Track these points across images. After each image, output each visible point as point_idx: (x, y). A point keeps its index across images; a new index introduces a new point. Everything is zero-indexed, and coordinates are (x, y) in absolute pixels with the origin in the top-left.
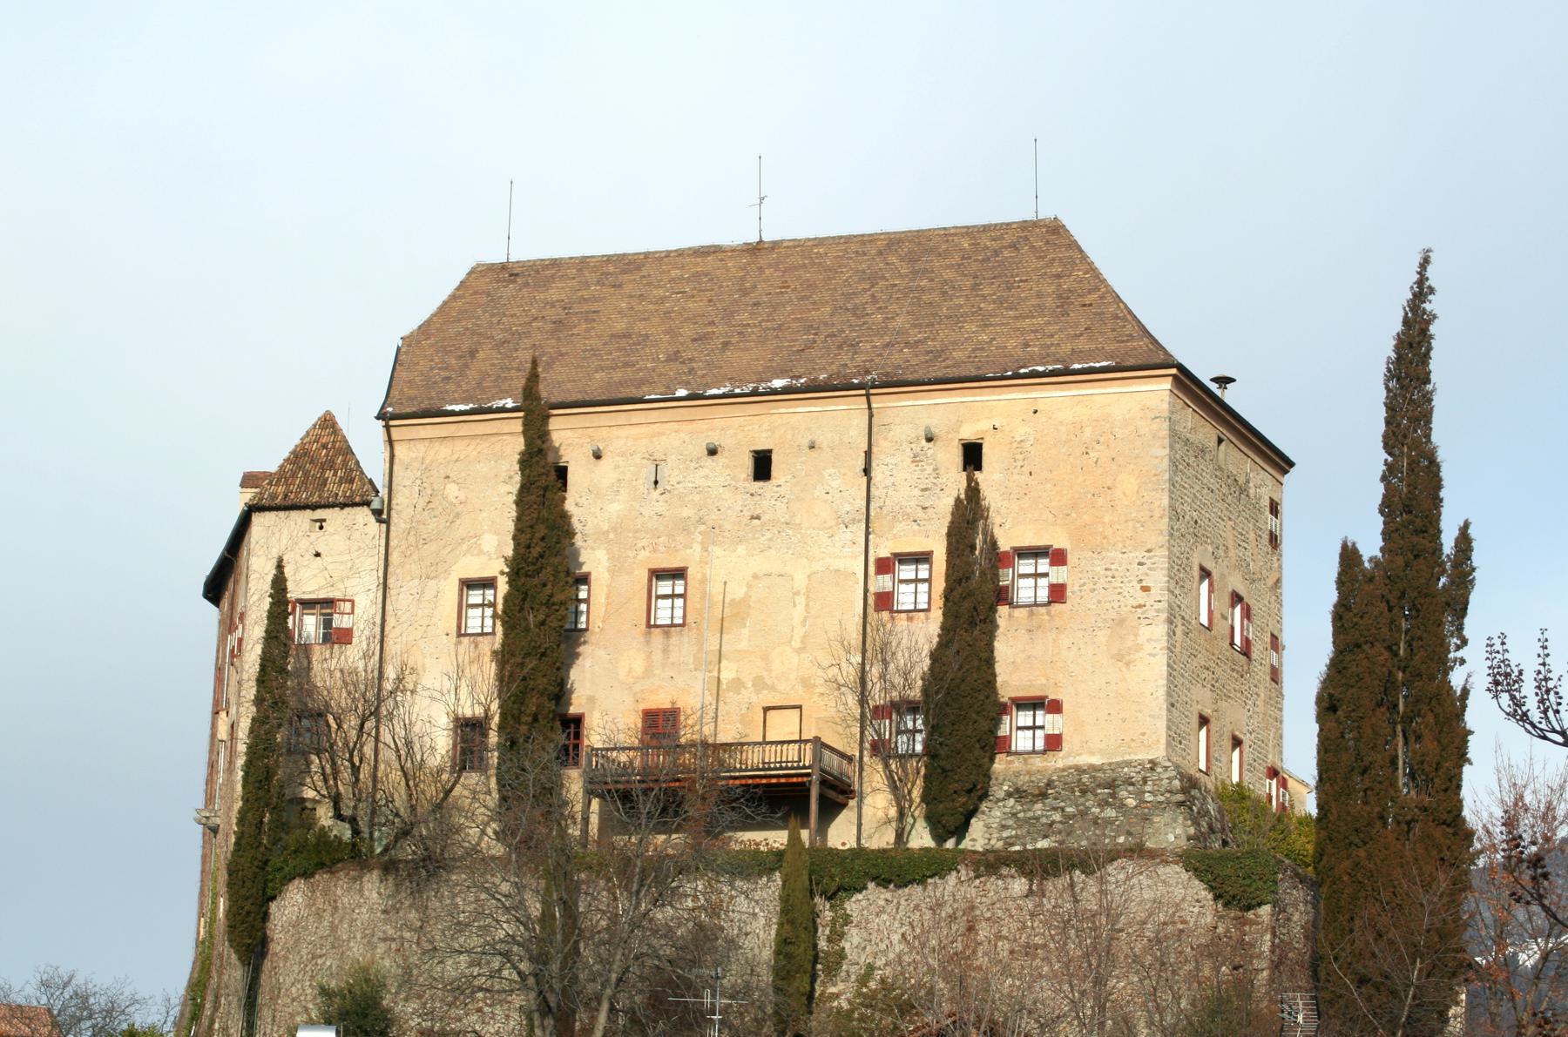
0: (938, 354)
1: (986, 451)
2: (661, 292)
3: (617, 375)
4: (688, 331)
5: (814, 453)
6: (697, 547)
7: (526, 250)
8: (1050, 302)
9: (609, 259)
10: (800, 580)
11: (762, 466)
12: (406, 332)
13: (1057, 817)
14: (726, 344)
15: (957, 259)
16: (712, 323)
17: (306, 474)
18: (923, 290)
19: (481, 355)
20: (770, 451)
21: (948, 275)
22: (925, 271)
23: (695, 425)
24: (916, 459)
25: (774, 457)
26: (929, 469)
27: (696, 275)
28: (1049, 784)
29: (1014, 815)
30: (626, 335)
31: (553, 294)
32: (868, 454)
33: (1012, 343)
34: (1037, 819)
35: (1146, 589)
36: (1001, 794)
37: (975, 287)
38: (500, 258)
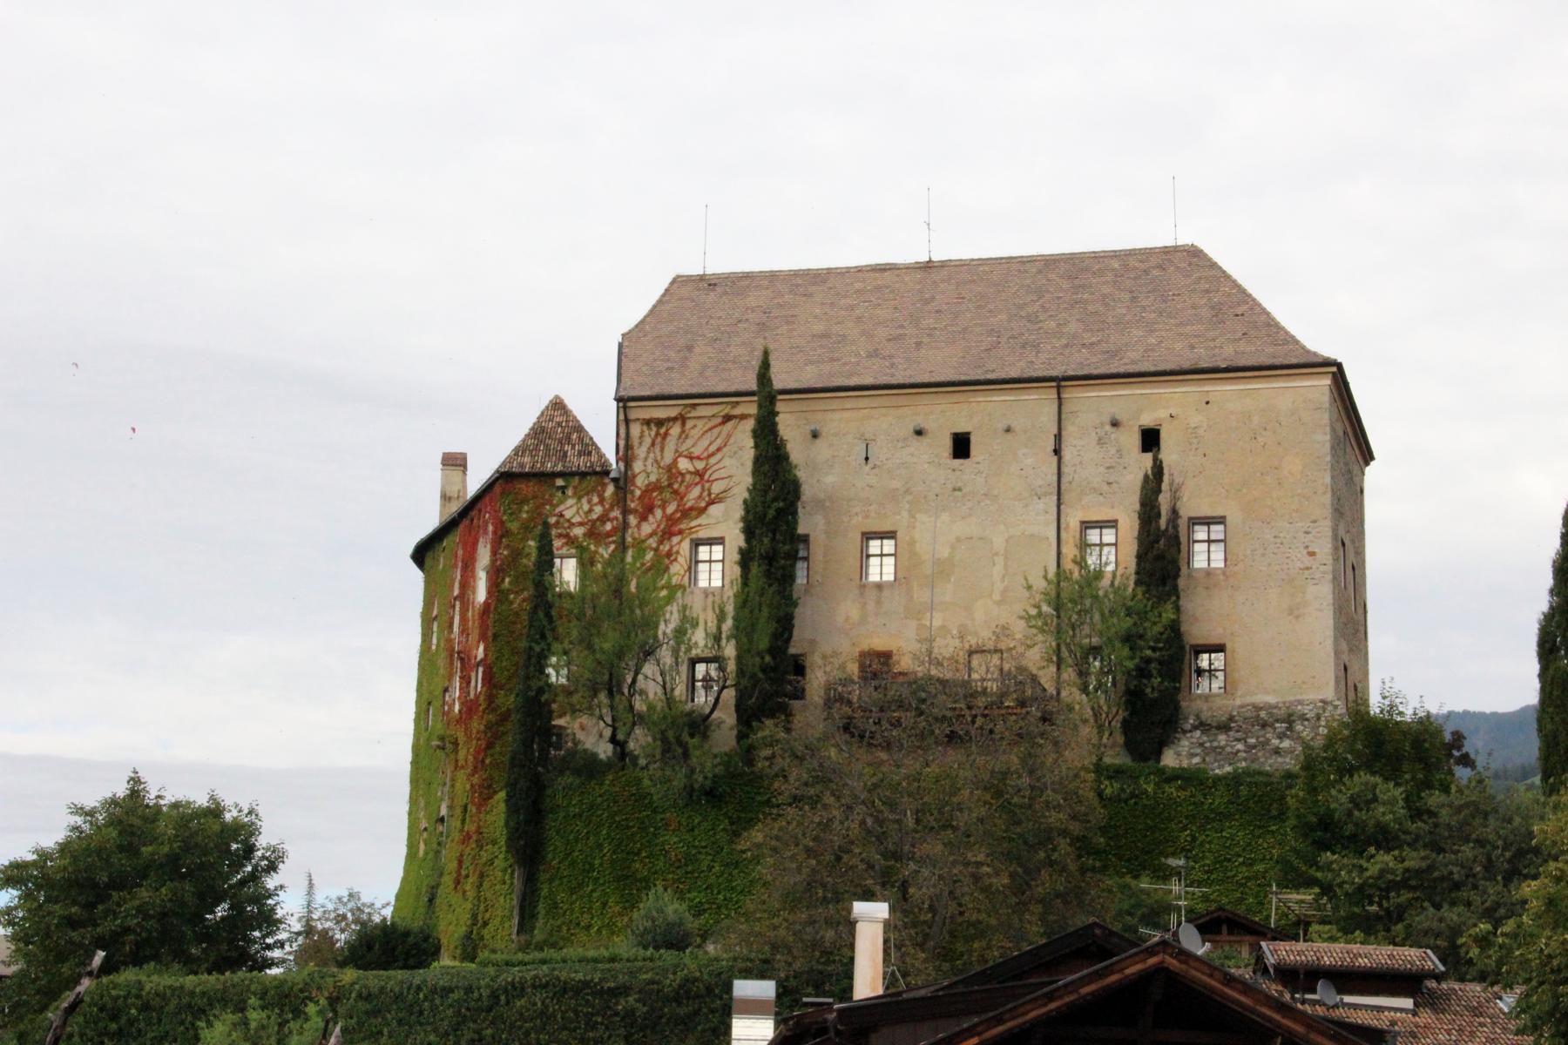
0: (1114, 354)
1: (1163, 435)
2: (849, 301)
3: (826, 368)
4: (882, 332)
5: (1009, 436)
6: (905, 514)
7: (719, 265)
8: (1205, 312)
9: (796, 274)
10: (999, 542)
11: (961, 446)
12: (625, 330)
13: (1240, 746)
14: (919, 344)
15: (1110, 277)
16: (902, 327)
17: (547, 446)
18: (1086, 302)
19: (697, 350)
20: (558, 405)
21: (1106, 290)
22: (1083, 286)
23: (900, 411)
24: (1100, 442)
25: (973, 439)
26: (1113, 451)
27: (878, 288)
28: (1231, 719)
29: (1201, 745)
30: (825, 336)
31: (751, 301)
32: (1058, 437)
33: (1178, 346)
34: (1223, 748)
35: (1312, 554)
36: (1188, 727)
37: (1134, 299)
38: (696, 270)
